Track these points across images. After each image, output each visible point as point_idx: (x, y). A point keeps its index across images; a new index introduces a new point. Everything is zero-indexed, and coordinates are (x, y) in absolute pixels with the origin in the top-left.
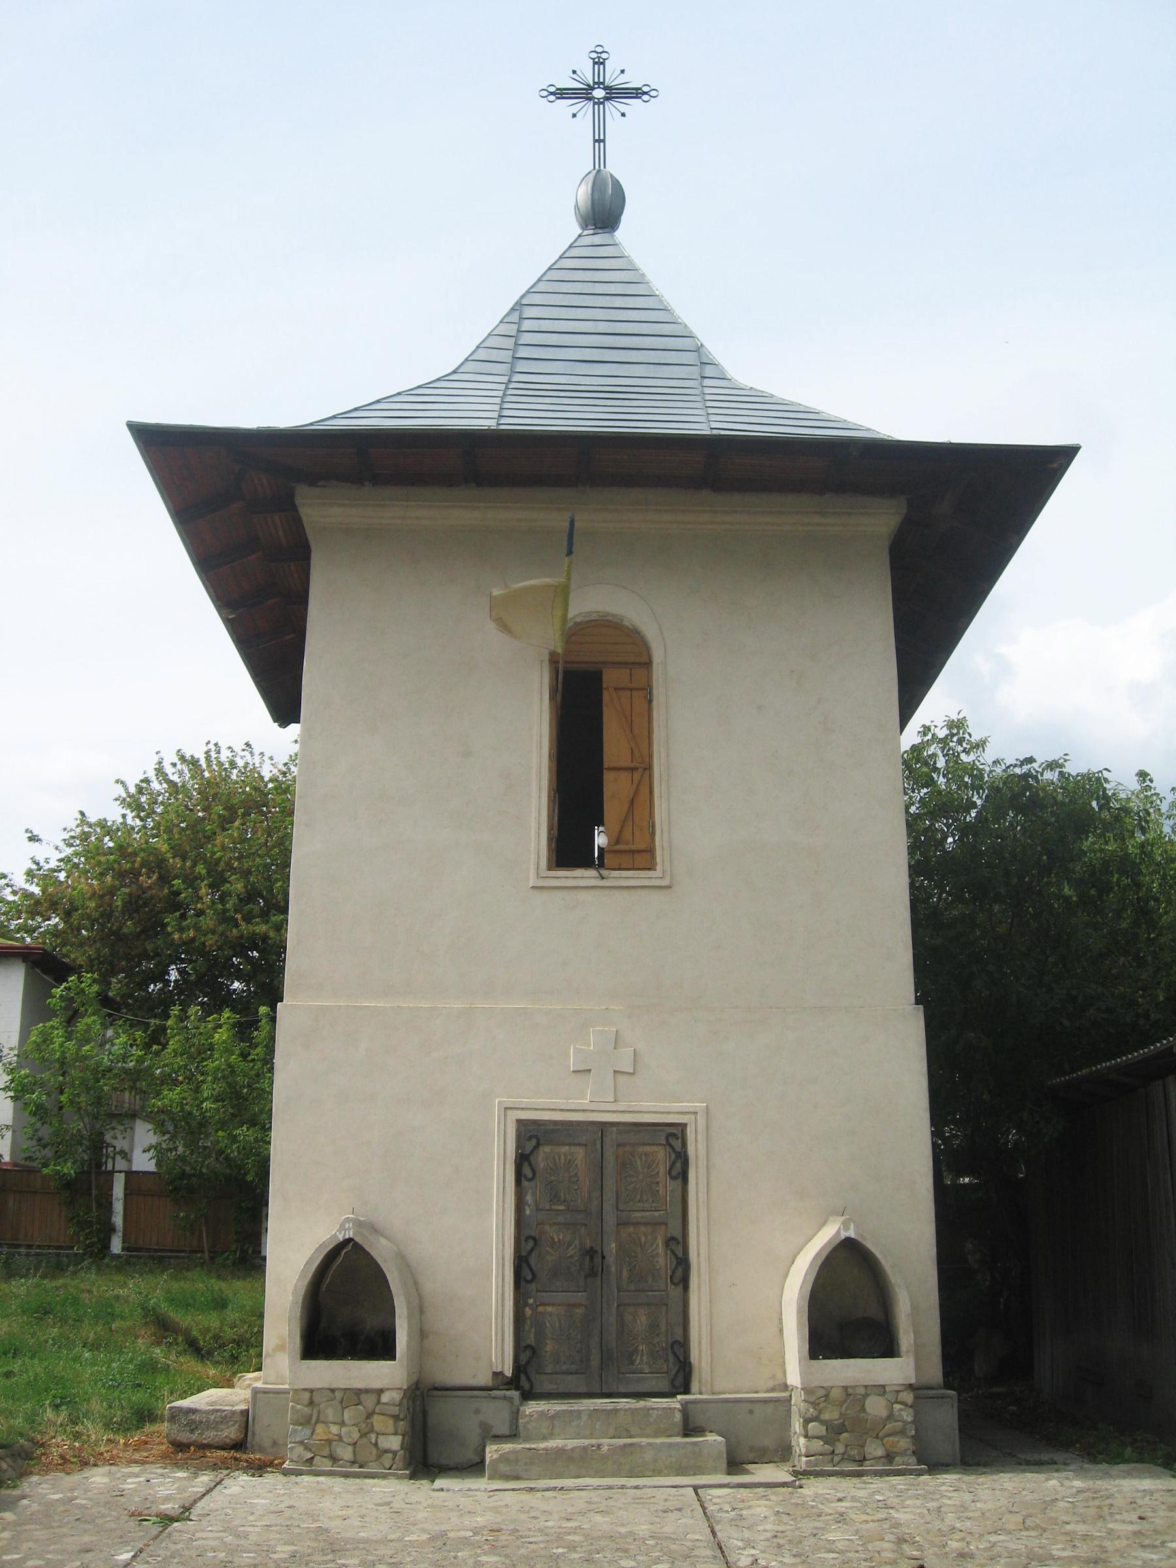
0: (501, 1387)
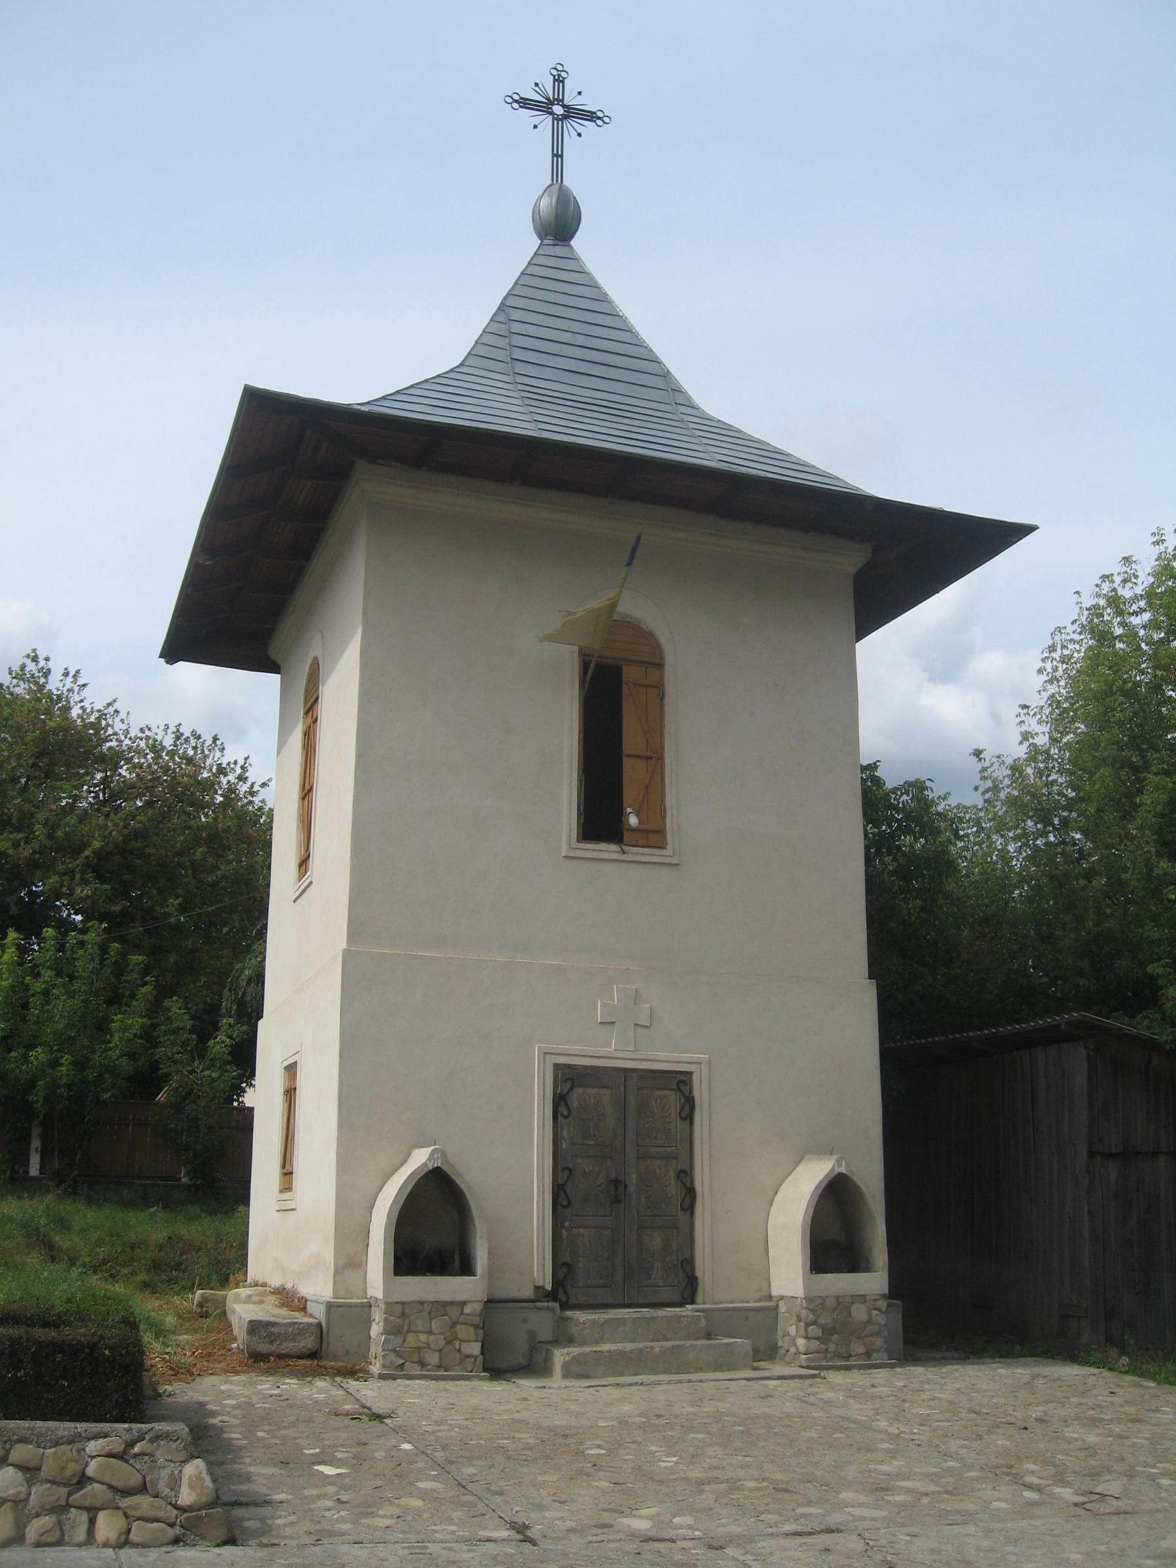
0: (543, 1300)
